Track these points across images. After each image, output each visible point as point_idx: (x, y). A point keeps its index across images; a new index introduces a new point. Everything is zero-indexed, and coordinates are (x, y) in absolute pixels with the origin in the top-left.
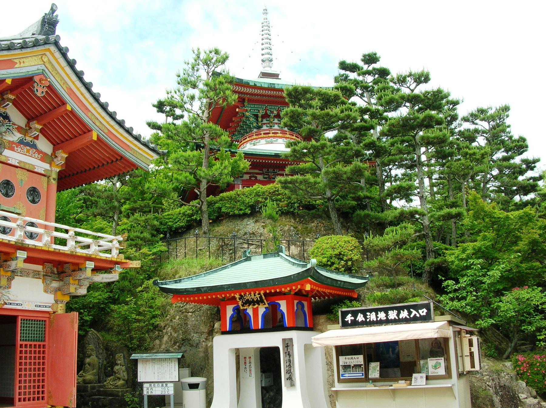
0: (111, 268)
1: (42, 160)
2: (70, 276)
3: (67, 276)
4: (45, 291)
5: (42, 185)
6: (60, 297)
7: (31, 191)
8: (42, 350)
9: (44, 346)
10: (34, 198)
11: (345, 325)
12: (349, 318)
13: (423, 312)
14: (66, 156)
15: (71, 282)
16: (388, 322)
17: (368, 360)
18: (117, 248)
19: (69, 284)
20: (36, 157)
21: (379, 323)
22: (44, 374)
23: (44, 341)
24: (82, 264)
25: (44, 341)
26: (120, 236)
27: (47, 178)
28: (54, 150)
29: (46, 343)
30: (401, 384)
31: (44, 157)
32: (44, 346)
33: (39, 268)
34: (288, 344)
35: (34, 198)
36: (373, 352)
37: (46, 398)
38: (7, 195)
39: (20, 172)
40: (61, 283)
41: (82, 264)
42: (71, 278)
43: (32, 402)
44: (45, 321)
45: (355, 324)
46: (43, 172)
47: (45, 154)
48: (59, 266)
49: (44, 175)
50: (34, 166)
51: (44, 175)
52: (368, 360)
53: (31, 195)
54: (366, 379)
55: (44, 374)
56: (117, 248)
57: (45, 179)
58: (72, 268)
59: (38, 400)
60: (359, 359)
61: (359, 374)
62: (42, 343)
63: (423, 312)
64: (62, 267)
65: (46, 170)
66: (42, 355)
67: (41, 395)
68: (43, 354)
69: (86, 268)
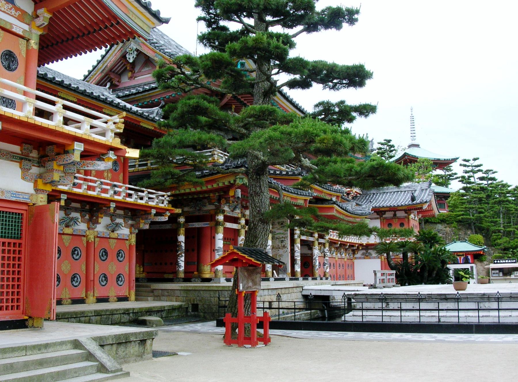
0: (103, 154)
1: (20, 19)
2: (53, 160)
3: (49, 161)
4: (23, 178)
5: (20, 50)
6: (41, 186)
7: (7, 54)
8: (17, 249)
9: (20, 244)
10: (9, 64)
11: (495, 263)
12: (496, 262)
13: (514, 261)
14: (51, 16)
15: (55, 167)
16: (505, 263)
17: (500, 272)
18: (112, 131)
19: (52, 170)
20: (13, 14)
21: (504, 263)
22: (20, 278)
23: (21, 238)
24: (70, 145)
25: (21, 238)
26: (116, 116)
27: (26, 41)
28: (36, 9)
29: (23, 242)
30: (508, 277)
31: (22, 16)
32: (20, 244)
33: (16, 149)
34: (472, 267)
35: (9, 64)
36: (500, 270)
37: (21, 307)
38: (8, 68)
39: (23, 42)
40: (42, 170)
41: (70, 145)
42: (55, 162)
43: (10, 311)
44: (22, 214)
45: (497, 263)
46: (21, 33)
47: (24, 12)
48: (41, 149)
49: (22, 37)
50: (12, 24)
51: (22, 37)
52: (500, 272)
53: (7, 59)
54: (499, 276)
55: (20, 278)
56: (112, 131)
57: (24, 42)
58: (56, 150)
59: (6, 309)
60: (498, 271)
61: (497, 275)
62: (17, 241)
63: (514, 261)
64: (44, 150)
65: (25, 31)
66: (17, 256)
67: (15, 304)
68: (19, 254)
69: (74, 150)
